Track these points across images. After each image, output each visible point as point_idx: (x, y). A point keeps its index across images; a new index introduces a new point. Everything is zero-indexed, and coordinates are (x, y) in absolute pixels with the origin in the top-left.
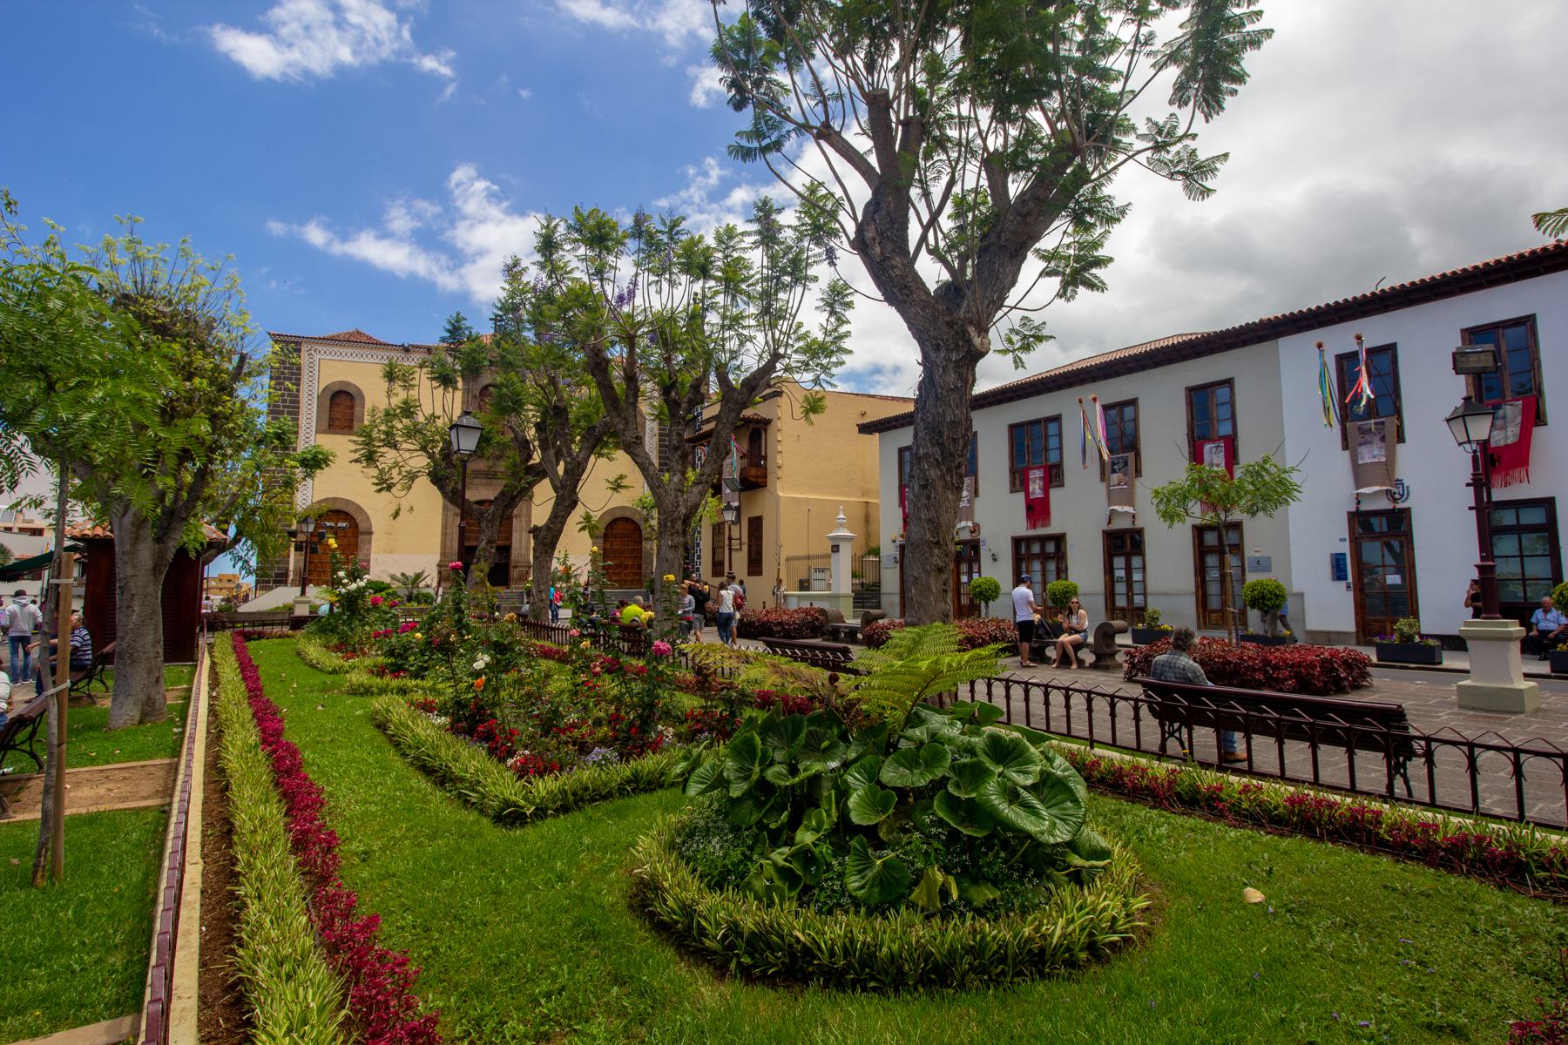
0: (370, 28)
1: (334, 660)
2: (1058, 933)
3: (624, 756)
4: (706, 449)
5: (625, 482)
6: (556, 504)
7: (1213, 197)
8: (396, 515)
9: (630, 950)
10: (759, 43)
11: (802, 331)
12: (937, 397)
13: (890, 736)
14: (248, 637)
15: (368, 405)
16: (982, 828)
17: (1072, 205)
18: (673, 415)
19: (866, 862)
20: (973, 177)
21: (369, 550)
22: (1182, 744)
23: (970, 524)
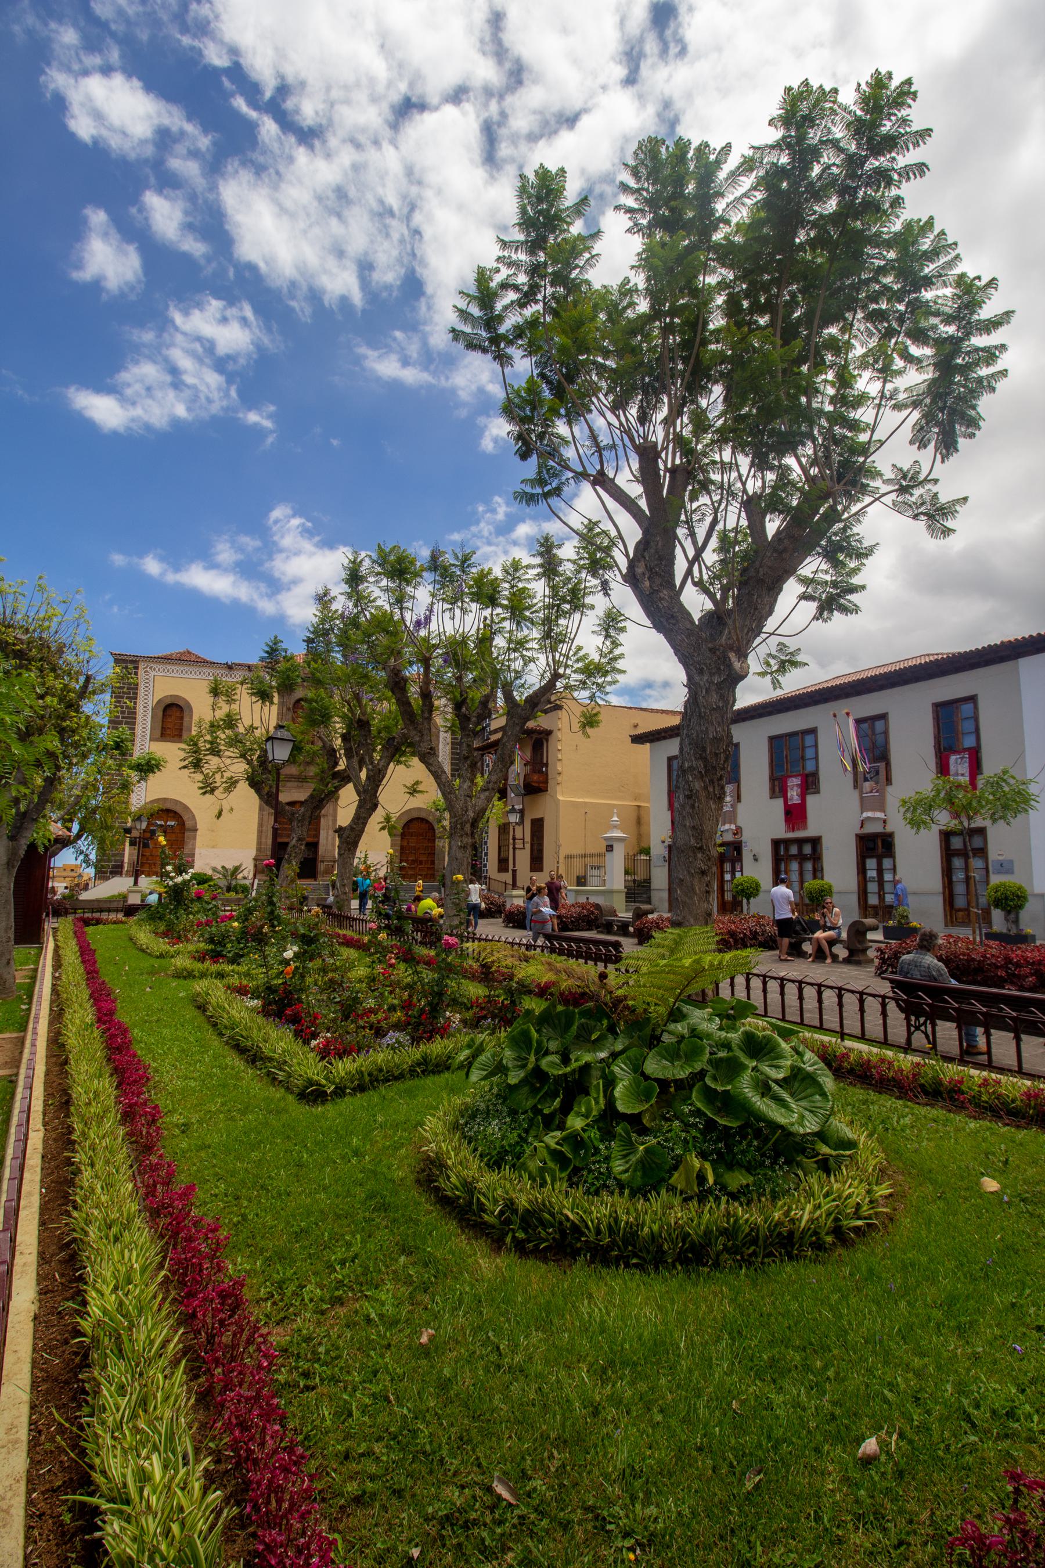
0: (203, 388)
1: (162, 945)
2: (806, 1217)
3: (416, 1040)
4: (493, 757)
5: (420, 788)
6: (359, 807)
7: (952, 536)
8: (219, 815)
9: (417, 1222)
10: (541, 402)
11: (581, 653)
12: (700, 716)
13: (654, 1030)
14: (87, 922)
15: (195, 718)
16: (737, 1118)
17: (823, 543)
18: (463, 728)
19: (630, 1147)
20: (734, 517)
21: (194, 845)
22: (927, 1037)
23: (733, 827)
